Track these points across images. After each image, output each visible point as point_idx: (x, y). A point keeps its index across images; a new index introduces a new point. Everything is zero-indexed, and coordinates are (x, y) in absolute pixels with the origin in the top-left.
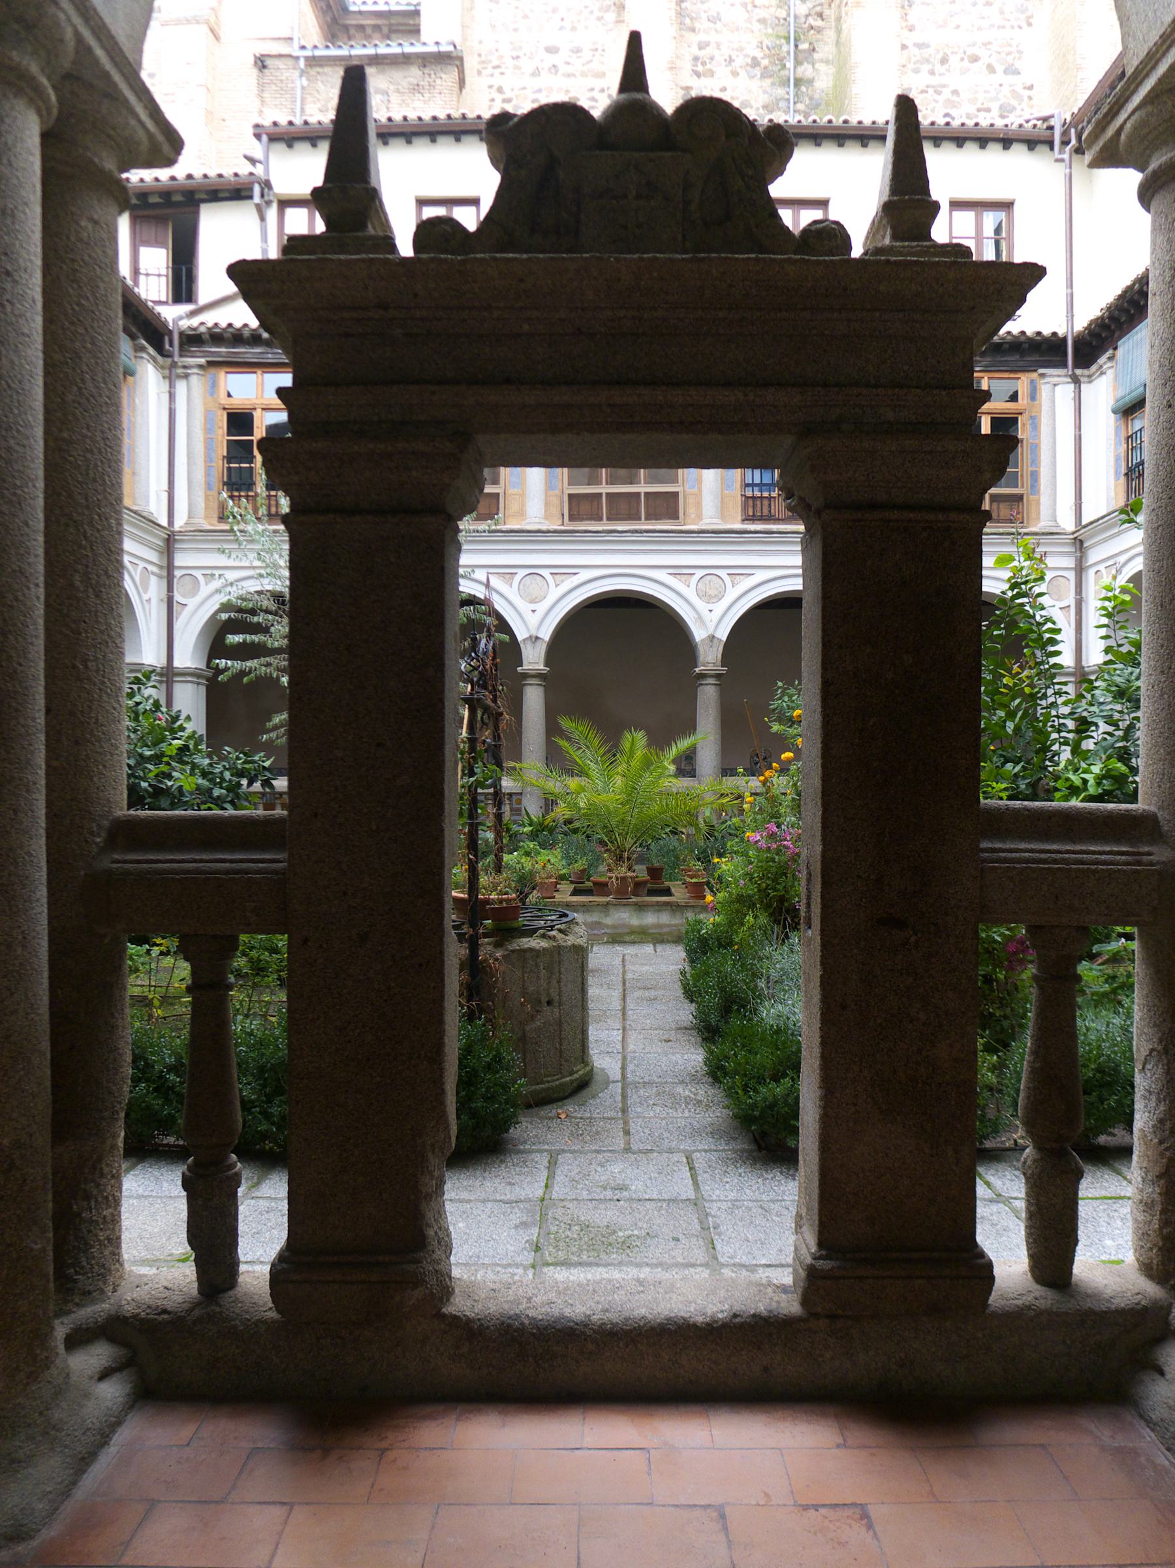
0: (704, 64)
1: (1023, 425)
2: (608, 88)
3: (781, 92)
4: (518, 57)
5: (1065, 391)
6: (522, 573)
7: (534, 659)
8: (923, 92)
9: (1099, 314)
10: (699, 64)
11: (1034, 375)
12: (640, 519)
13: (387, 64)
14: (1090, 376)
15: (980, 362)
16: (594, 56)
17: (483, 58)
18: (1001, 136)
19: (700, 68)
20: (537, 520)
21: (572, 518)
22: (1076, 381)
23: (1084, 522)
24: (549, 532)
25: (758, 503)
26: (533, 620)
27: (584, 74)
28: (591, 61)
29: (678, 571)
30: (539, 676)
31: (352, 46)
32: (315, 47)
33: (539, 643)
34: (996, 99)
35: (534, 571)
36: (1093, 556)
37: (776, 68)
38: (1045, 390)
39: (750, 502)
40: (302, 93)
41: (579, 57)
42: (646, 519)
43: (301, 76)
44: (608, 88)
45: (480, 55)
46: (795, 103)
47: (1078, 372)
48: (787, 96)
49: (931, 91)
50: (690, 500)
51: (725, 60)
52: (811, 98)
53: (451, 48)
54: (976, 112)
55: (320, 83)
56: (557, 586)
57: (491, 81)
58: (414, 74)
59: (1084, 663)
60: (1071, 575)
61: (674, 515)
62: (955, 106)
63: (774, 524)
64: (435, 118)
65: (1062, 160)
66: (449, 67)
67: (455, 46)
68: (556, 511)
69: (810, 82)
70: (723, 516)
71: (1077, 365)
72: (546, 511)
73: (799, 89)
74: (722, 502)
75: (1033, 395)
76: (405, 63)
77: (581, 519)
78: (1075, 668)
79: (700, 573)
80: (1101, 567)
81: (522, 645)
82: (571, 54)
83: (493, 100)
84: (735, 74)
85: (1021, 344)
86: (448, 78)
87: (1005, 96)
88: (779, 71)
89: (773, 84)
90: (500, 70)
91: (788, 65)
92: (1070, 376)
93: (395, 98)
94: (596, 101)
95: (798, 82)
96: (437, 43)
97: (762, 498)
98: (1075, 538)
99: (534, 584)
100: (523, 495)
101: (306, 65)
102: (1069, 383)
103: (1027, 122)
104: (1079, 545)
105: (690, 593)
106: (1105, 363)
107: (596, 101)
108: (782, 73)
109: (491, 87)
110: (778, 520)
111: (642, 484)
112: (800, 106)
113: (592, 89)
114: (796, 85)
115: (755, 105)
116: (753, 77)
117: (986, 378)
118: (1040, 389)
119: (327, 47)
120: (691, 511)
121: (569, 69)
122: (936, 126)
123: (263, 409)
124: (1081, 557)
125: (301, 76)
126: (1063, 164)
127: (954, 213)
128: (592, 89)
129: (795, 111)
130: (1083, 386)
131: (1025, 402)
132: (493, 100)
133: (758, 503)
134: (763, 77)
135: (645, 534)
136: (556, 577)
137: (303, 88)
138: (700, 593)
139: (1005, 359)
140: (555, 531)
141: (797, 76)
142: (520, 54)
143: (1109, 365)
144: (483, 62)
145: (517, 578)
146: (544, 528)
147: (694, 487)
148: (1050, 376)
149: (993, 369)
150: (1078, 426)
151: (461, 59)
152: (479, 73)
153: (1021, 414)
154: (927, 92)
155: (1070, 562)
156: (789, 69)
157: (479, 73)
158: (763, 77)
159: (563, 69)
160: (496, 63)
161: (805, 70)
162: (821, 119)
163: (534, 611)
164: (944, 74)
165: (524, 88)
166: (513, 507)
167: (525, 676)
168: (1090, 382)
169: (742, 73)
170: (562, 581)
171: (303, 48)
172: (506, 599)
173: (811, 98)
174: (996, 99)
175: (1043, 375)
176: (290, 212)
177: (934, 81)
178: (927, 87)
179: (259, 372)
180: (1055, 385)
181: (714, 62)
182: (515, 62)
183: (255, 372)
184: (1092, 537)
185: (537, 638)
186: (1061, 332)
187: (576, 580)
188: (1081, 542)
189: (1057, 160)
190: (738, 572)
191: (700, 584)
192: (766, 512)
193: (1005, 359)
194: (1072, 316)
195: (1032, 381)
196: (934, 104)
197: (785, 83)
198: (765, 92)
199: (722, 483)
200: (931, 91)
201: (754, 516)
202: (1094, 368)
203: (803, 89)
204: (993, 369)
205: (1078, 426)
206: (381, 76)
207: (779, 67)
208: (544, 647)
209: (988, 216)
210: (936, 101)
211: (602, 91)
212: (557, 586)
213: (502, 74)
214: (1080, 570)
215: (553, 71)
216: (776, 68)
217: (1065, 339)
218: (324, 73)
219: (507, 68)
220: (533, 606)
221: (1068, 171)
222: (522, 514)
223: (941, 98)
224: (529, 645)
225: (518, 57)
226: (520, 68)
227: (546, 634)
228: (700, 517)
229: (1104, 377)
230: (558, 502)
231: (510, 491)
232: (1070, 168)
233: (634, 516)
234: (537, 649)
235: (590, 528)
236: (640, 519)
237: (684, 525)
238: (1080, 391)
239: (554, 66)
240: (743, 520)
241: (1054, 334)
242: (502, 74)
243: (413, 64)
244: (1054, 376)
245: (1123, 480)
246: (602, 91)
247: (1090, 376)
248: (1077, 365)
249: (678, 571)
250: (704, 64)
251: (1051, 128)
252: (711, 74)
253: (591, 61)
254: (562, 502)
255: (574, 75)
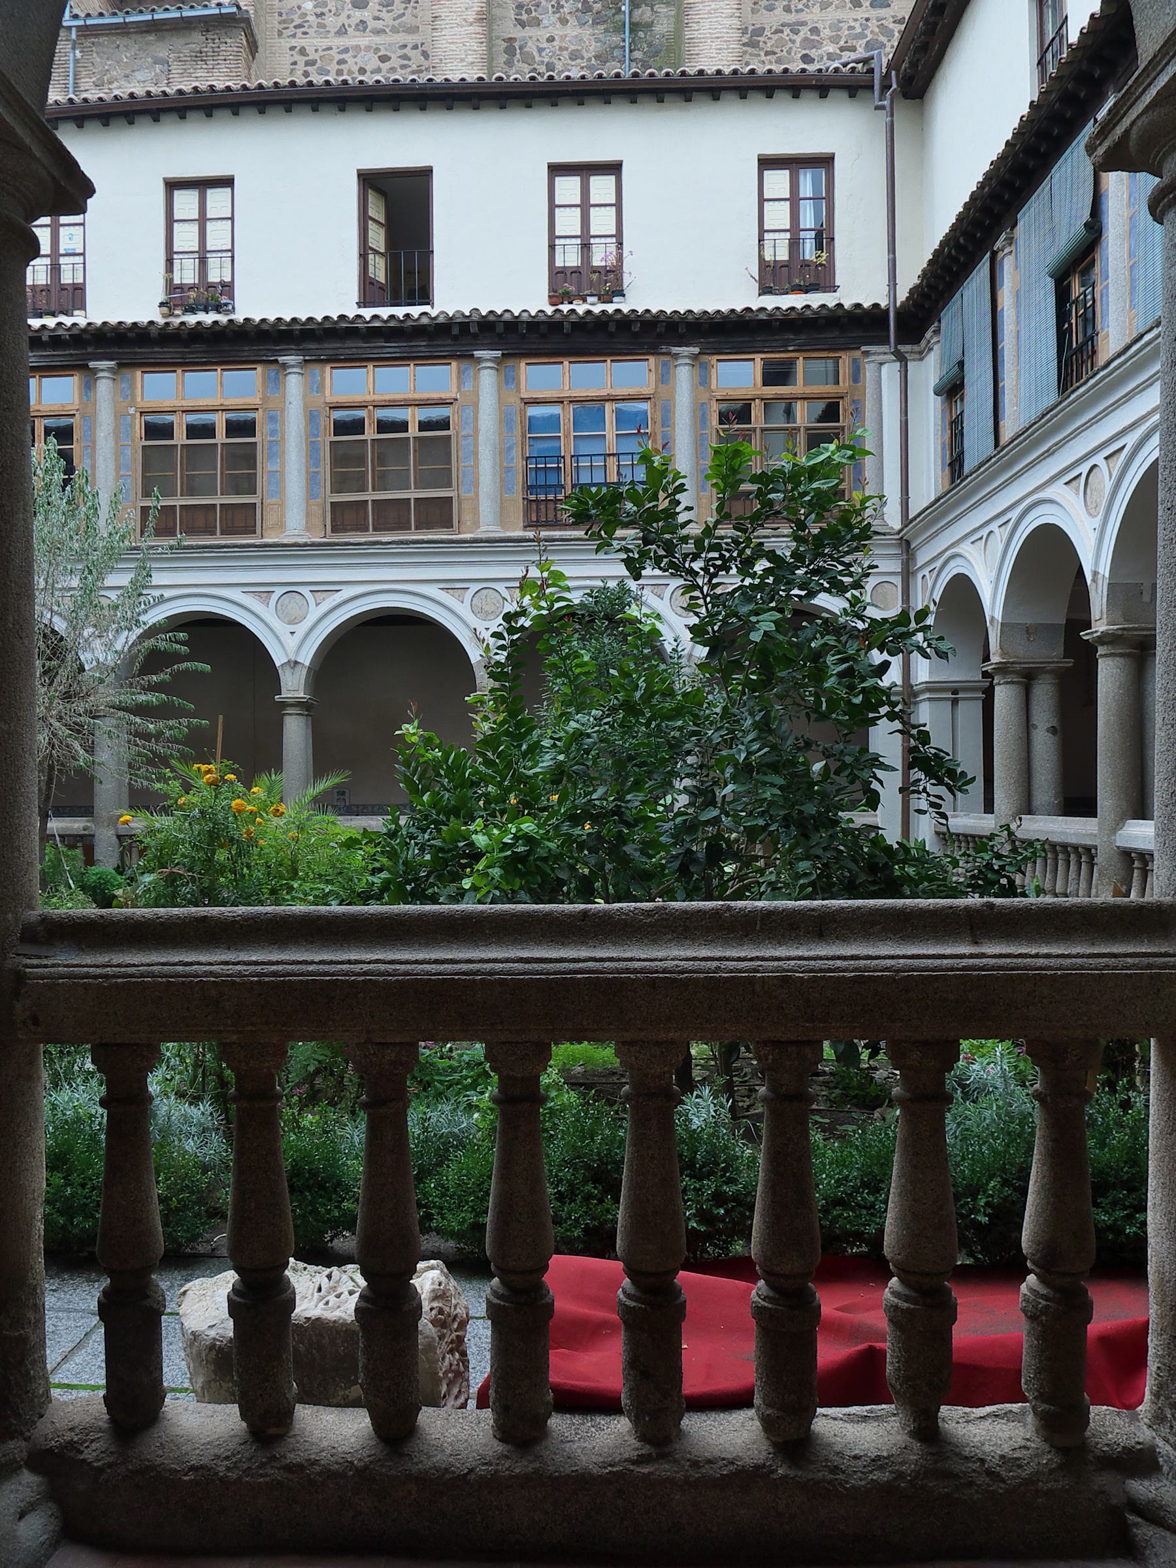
0: (529, 12)
1: (845, 410)
2: (422, 44)
3: (616, 39)
4: (323, 14)
5: (890, 373)
6: (279, 591)
7: (293, 686)
8: (777, 32)
9: (917, 281)
10: (523, 12)
11: (857, 354)
12: (367, 530)
13: (167, 30)
14: (921, 353)
15: (794, 340)
16: (406, 8)
17: (284, 17)
18: (814, 82)
19: (525, 17)
20: (296, 532)
21: (335, 529)
22: (902, 358)
23: (910, 517)
24: (306, 545)
25: (543, 507)
26: (292, 643)
27: (395, 30)
28: (404, 14)
29: (450, 585)
30: (299, 704)
31: (127, 13)
32: (88, 15)
33: (298, 668)
34: (861, 36)
35: (292, 590)
36: (922, 558)
37: (610, 13)
38: (869, 371)
39: (534, 506)
40: (75, 67)
41: (388, 11)
42: (375, 529)
43: (74, 48)
44: (422, 44)
45: (280, 14)
46: (631, 51)
47: (902, 348)
48: (622, 44)
49: (787, 31)
50: (466, 505)
51: (553, 6)
52: (650, 45)
53: (234, 9)
54: (838, 51)
55: (95, 55)
56: (317, 605)
57: (294, 42)
58: (197, 40)
59: (913, 682)
60: (898, 580)
61: (447, 523)
62: (815, 47)
63: (560, 530)
64: (132, 95)
65: (883, 108)
66: (234, 30)
67: (239, 7)
68: (317, 522)
69: (650, 25)
70: (503, 523)
71: (900, 340)
72: (307, 522)
73: (636, 35)
74: (501, 508)
75: (856, 375)
76: (186, 28)
77: (346, 530)
78: (903, 687)
79: (475, 587)
80: (926, 572)
81: (280, 671)
82: (381, 8)
83: (295, 63)
84: (564, 21)
85: (539, 323)
86: (234, 43)
87: (872, 32)
88: (614, 15)
89: (606, 30)
90: (303, 30)
91: (623, 8)
92: (892, 353)
93: (176, 68)
94: (410, 59)
95: (635, 27)
96: (219, 5)
97: (546, 501)
98: (902, 538)
99: (293, 602)
100: (282, 505)
101: (77, 36)
102: (894, 361)
103: (845, 65)
104: (906, 548)
105: (464, 610)
106: (932, 337)
107: (410, 59)
108: (617, 17)
109: (292, 48)
110: (565, 526)
111: (179, 497)
112: (638, 55)
113: (405, 46)
114: (631, 31)
115: (586, 55)
116: (584, 24)
117: (801, 358)
118: (865, 369)
119: (115, 14)
120: (467, 517)
121: (379, 24)
122: (807, 73)
123: (374, 406)
124: (908, 560)
125: (74, 48)
126: (884, 112)
127: (766, 173)
128: (405, 46)
129: (631, 60)
130: (909, 363)
131: (847, 385)
132: (295, 63)
133: (543, 507)
134: (595, 23)
135: (411, 546)
136: (316, 594)
137: (76, 61)
138: (475, 609)
139: (822, 336)
140: (313, 545)
141: (633, 20)
142: (325, 10)
143: (935, 339)
144: (284, 22)
145: (275, 597)
146: (301, 540)
147: (470, 491)
148: (874, 354)
149: (808, 348)
150: (905, 411)
151: (247, 21)
152: (280, 34)
153: (842, 397)
154: (782, 32)
155: (895, 566)
156: (624, 12)
157: (280, 34)
158: (595, 23)
159: (372, 24)
160: (298, 22)
161: (643, 13)
162: (508, 77)
163: (292, 633)
164: (802, 10)
165: (330, 48)
166: (271, 518)
167: (284, 705)
168: (921, 359)
169: (572, 21)
170: (324, 599)
171: (76, 17)
172: (262, 620)
173: (650, 45)
174: (861, 36)
175: (867, 354)
176: (180, 196)
177: (791, 18)
178: (782, 25)
179: (179, 371)
180: (881, 364)
181: (540, 9)
182: (319, 20)
183: (175, 371)
184: (916, 537)
185: (296, 663)
186: (883, 304)
187: (338, 598)
188: (908, 543)
189: (877, 108)
190: (322, 589)
191: (475, 599)
192: (551, 516)
193: (822, 336)
194: (895, 284)
195: (855, 361)
196: (790, 45)
197: (620, 29)
198: (598, 40)
199: (501, 486)
200: (787, 31)
201: (537, 521)
202: (923, 342)
203: (641, 34)
204: (808, 348)
205: (905, 411)
206: (160, 44)
207: (613, 11)
208: (305, 672)
209: (805, 175)
210: (793, 42)
211: (415, 47)
212: (317, 605)
213: (305, 33)
214: (907, 574)
215: (361, 28)
216: (610, 13)
217: (887, 311)
218: (100, 44)
219: (310, 27)
220: (292, 628)
221: (889, 119)
222: (281, 526)
223: (798, 39)
224: (288, 670)
225: (323, 14)
226: (324, 26)
227: (306, 658)
228: (476, 524)
229: (932, 353)
230: (320, 512)
231: (267, 502)
232: (892, 115)
233: (404, 526)
234: (297, 675)
235: (352, 540)
236: (367, 530)
237: (459, 533)
238: (906, 371)
239: (361, 21)
240: (525, 527)
241: (876, 306)
242: (305, 33)
243: (195, 28)
244: (879, 354)
245: (947, 469)
246: (415, 47)
247: (921, 353)
248: (900, 340)
249: (450, 585)
250: (529, 12)
251: (871, 71)
252: (537, 23)
253: (404, 14)
254: (324, 512)
255: (384, 31)
